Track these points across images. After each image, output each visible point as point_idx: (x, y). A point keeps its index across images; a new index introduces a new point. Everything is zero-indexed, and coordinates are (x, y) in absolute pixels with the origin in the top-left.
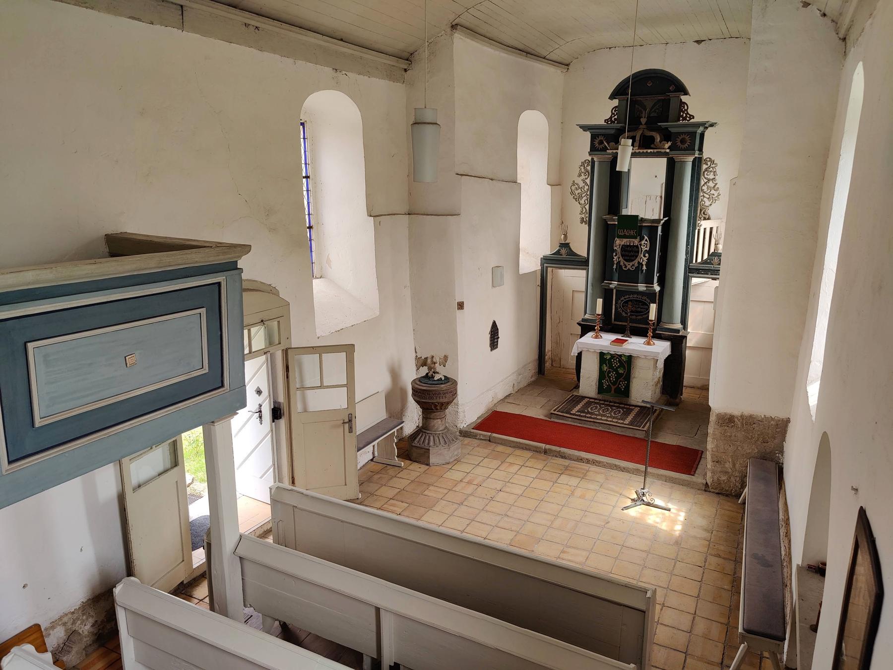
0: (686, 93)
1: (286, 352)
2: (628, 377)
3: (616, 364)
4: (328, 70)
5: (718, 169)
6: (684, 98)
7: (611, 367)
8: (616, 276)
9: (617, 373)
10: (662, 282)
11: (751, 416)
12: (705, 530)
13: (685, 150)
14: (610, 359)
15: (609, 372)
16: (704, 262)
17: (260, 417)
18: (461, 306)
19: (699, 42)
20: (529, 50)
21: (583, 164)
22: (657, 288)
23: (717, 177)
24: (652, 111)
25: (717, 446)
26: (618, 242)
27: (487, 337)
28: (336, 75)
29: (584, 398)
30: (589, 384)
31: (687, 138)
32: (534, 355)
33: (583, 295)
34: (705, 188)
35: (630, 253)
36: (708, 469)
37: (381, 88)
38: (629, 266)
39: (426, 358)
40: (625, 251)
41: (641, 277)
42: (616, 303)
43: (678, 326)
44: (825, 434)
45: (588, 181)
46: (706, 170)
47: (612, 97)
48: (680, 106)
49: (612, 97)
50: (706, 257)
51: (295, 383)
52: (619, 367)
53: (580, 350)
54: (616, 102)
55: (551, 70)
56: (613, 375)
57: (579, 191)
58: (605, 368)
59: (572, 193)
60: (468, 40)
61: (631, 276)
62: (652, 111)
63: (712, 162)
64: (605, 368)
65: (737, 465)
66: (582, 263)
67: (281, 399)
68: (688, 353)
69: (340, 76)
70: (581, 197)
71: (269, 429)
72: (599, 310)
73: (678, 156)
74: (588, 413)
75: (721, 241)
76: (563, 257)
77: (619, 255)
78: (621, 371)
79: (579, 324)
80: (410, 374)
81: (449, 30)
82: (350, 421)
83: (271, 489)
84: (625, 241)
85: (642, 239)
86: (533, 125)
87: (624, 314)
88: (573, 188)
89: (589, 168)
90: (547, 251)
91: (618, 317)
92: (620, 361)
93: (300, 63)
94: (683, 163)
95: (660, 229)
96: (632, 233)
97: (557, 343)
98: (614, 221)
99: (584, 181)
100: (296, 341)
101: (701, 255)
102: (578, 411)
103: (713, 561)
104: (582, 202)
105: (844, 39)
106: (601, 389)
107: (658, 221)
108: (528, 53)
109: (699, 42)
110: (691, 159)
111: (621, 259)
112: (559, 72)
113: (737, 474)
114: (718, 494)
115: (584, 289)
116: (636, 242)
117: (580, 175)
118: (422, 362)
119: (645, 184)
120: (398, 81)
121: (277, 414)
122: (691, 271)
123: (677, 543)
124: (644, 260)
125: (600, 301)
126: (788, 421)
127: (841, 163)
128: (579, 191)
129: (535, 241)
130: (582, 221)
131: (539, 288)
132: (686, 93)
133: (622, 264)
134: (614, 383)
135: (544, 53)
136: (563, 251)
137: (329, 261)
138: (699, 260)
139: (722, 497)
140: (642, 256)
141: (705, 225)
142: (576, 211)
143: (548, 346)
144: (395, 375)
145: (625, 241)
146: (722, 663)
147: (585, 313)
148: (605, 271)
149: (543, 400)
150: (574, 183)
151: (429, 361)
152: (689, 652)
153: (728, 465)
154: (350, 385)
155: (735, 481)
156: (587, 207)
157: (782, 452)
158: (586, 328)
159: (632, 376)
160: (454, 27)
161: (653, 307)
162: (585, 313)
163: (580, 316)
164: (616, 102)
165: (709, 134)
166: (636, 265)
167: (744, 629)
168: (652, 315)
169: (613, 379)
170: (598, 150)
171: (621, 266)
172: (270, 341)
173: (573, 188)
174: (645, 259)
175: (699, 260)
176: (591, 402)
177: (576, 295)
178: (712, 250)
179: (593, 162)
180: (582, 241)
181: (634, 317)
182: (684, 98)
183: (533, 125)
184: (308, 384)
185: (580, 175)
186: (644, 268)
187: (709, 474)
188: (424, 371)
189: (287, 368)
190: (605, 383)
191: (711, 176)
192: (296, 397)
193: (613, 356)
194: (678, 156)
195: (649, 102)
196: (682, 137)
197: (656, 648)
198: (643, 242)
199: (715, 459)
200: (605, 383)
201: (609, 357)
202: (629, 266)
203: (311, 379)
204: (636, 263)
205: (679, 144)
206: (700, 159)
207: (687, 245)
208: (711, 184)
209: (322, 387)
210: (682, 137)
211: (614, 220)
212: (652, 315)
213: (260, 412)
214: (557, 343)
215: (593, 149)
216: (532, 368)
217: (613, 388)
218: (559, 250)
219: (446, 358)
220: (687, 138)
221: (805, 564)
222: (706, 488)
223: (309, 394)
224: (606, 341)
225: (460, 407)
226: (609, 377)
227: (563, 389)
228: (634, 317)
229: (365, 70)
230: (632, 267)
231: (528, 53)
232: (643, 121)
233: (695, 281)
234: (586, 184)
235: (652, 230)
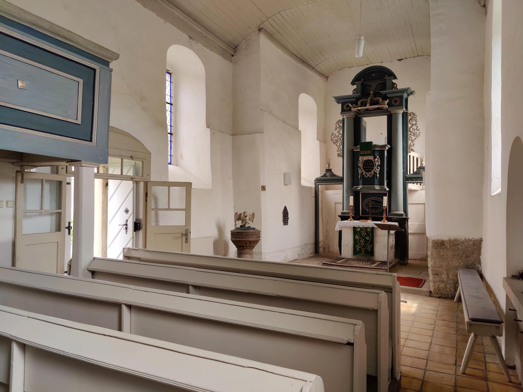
0: (395, 78)
1: (146, 184)
2: (372, 242)
4: (185, 37)
5: (418, 118)
6: (394, 81)
7: (361, 236)
8: (361, 182)
9: (365, 239)
10: (389, 185)
11: (456, 240)
12: (433, 310)
13: (397, 106)
14: (360, 231)
15: (360, 239)
16: (414, 173)
17: (126, 229)
18: (263, 188)
19: (400, 60)
20: (304, 60)
21: (338, 122)
22: (388, 189)
23: (417, 123)
24: (376, 90)
25: (435, 263)
26: (362, 159)
27: (281, 215)
28: (190, 40)
30: (347, 250)
31: (398, 99)
32: (312, 240)
33: (341, 205)
34: (411, 130)
35: (369, 165)
36: (430, 286)
37: (217, 59)
39: (241, 214)
40: (366, 166)
41: (376, 181)
42: (362, 203)
43: (402, 212)
44: (507, 295)
45: (341, 132)
46: (411, 119)
47: (353, 83)
48: (392, 85)
49: (353, 83)
50: (415, 170)
51: (151, 204)
54: (355, 87)
55: (317, 77)
56: (362, 241)
57: (336, 138)
58: (357, 237)
59: (332, 140)
60: (268, 41)
61: (369, 182)
62: (376, 90)
64: (357, 237)
65: (450, 276)
66: (340, 180)
67: (141, 217)
68: (410, 237)
69: (193, 42)
70: (337, 141)
71: (131, 236)
72: (351, 203)
73: (393, 110)
75: (424, 160)
76: (328, 178)
77: (362, 168)
78: (367, 238)
79: (339, 216)
80: (230, 226)
81: (257, 32)
82: (186, 235)
83: (124, 249)
84: (366, 158)
85: (375, 158)
86: (307, 103)
87: (367, 210)
88: (332, 137)
89: (341, 124)
90: (318, 175)
91: (364, 211)
92: (366, 232)
93: (169, 25)
94: (397, 114)
95: (386, 152)
97: (327, 236)
98: (358, 149)
99: (338, 132)
100: (154, 178)
101: (412, 169)
103: (441, 323)
104: (338, 144)
105: (484, 6)
106: (355, 252)
107: (384, 146)
108: (303, 62)
109: (400, 60)
110: (402, 112)
111: (363, 171)
112: (322, 80)
113: (451, 282)
114: (439, 298)
115: (341, 201)
116: (371, 158)
117: (336, 129)
118: (238, 217)
119: (375, 130)
120: (228, 60)
121: (137, 227)
122: (407, 179)
123: (414, 315)
124: (378, 171)
125: (352, 198)
126: (480, 241)
127: (493, 53)
128: (336, 138)
129: (310, 171)
130: (339, 155)
131: (314, 199)
132: (395, 78)
133: (364, 174)
134: (364, 247)
135: (314, 66)
136: (328, 174)
137: (182, 156)
138: (412, 172)
139: (442, 300)
140: (376, 168)
141: (411, 154)
142: (335, 149)
143: (321, 238)
144: (221, 230)
145: (366, 158)
146: (456, 364)
147: (343, 209)
148: (354, 179)
151: (242, 215)
152: (429, 359)
153: (444, 276)
154: (187, 210)
155: (450, 287)
156: (341, 147)
157: (480, 263)
159: (375, 241)
160: (260, 30)
161: (385, 199)
163: (339, 210)
164: (355, 87)
165: (410, 98)
166: (373, 174)
167: (470, 319)
168: (385, 203)
170: (346, 111)
172: (136, 172)
173: (332, 137)
174: (378, 170)
175: (412, 172)
177: (337, 205)
178: (419, 166)
180: (339, 167)
181: (374, 211)
182: (394, 81)
183: (307, 103)
184: (160, 207)
185: (336, 129)
186: (378, 175)
187: (431, 284)
188: (239, 224)
189: (147, 194)
191: (414, 122)
192: (152, 214)
194: (393, 110)
195: (374, 85)
196: (395, 99)
197: (403, 357)
198: (376, 160)
199: (434, 272)
201: (359, 230)
202: (369, 175)
203: (163, 204)
204: (372, 172)
205: (393, 103)
206: (407, 113)
207: (403, 169)
208: (414, 127)
209: (169, 209)
210: (395, 99)
211: (357, 149)
212: (385, 203)
213: (127, 225)
214: (327, 236)
215: (343, 111)
216: (310, 248)
218: (325, 174)
219: (253, 214)
220: (398, 99)
221: (510, 275)
222: (430, 294)
223: (161, 213)
225: (263, 255)
226: (360, 243)
228: (374, 211)
229: (208, 45)
230: (370, 178)
231: (303, 62)
232: (372, 93)
233: (411, 186)
235: (381, 153)
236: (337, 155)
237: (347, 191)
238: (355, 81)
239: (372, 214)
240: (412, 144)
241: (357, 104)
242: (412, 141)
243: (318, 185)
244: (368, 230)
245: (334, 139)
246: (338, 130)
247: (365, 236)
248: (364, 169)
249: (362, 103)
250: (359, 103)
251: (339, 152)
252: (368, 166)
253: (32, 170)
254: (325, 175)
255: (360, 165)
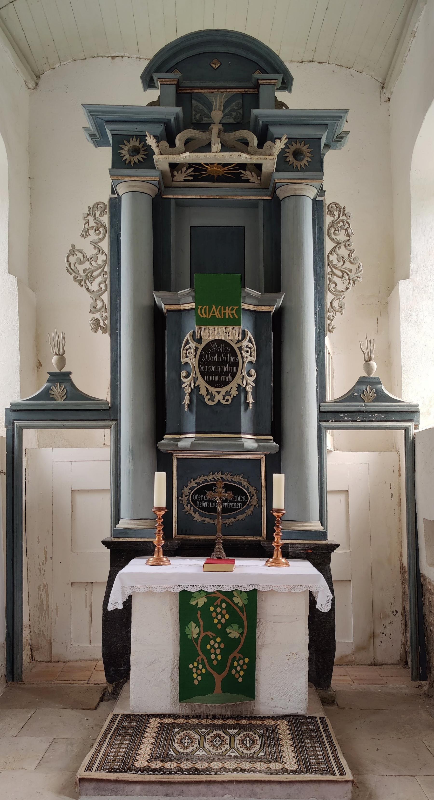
2: (248, 647)
3: (219, 617)
7: (209, 625)
8: (191, 420)
13: (302, 170)
14: (207, 606)
15: (206, 640)
16: (349, 397)
21: (92, 211)
29: (144, 718)
30: (153, 683)
31: (304, 149)
34: (333, 258)
38: (219, 395)
40: (209, 363)
41: (246, 419)
43: (316, 526)
45: (105, 245)
46: (333, 224)
52: (228, 623)
53: (128, 592)
56: (215, 644)
57: (87, 265)
58: (194, 631)
59: (71, 270)
61: (219, 421)
63: (342, 210)
64: (194, 631)
66: (107, 414)
74: (180, 757)
77: (195, 372)
78: (234, 633)
79: (105, 543)
84: (211, 334)
88: (73, 259)
89: (105, 219)
92: (230, 609)
96: (228, 312)
99: (95, 244)
101: (336, 390)
102: (334, 774)
104: (94, 287)
106: (187, 688)
111: (201, 382)
117: (85, 234)
125: (160, 478)
128: (87, 265)
130: (96, 326)
133: (203, 391)
134: (220, 667)
136: (58, 390)
140: (244, 373)
147: (116, 518)
149: (35, 744)
150: (73, 251)
156: (106, 297)
158: (122, 552)
159: (259, 642)
162: (116, 518)
166: (234, 392)
169: (216, 656)
170: (129, 166)
171: (201, 398)
174: (251, 380)
176: (169, 725)
179: (115, 206)
185: (85, 234)
186: (250, 399)
190: (198, 670)
191: (341, 236)
193: (212, 598)
200: (198, 670)
201: (201, 601)
202: (219, 395)
204: (232, 387)
206: (321, 202)
208: (343, 251)
215: (118, 163)
217: (218, 679)
224: (188, 570)
227: (76, 706)
234: (100, 250)
236: (89, 325)
237: (133, 453)
238: (157, 71)
239: (227, 530)
240: (336, 304)
241: (172, 144)
242: (337, 294)
243: (21, 428)
244: (236, 600)
245: (81, 268)
246: (93, 236)
247: (225, 626)
248: (203, 374)
249: (187, 142)
250: (179, 140)
251: (98, 316)
252: (219, 364)
253: (181, 437)
254: (46, 395)
255: (190, 357)
